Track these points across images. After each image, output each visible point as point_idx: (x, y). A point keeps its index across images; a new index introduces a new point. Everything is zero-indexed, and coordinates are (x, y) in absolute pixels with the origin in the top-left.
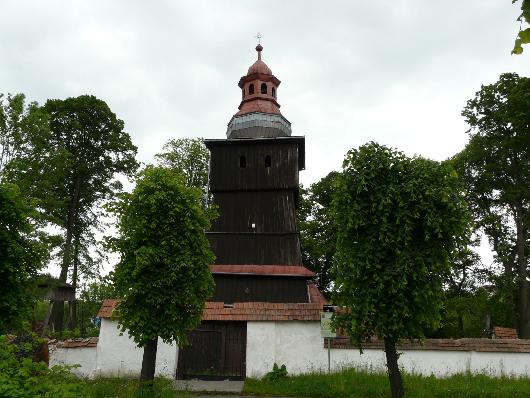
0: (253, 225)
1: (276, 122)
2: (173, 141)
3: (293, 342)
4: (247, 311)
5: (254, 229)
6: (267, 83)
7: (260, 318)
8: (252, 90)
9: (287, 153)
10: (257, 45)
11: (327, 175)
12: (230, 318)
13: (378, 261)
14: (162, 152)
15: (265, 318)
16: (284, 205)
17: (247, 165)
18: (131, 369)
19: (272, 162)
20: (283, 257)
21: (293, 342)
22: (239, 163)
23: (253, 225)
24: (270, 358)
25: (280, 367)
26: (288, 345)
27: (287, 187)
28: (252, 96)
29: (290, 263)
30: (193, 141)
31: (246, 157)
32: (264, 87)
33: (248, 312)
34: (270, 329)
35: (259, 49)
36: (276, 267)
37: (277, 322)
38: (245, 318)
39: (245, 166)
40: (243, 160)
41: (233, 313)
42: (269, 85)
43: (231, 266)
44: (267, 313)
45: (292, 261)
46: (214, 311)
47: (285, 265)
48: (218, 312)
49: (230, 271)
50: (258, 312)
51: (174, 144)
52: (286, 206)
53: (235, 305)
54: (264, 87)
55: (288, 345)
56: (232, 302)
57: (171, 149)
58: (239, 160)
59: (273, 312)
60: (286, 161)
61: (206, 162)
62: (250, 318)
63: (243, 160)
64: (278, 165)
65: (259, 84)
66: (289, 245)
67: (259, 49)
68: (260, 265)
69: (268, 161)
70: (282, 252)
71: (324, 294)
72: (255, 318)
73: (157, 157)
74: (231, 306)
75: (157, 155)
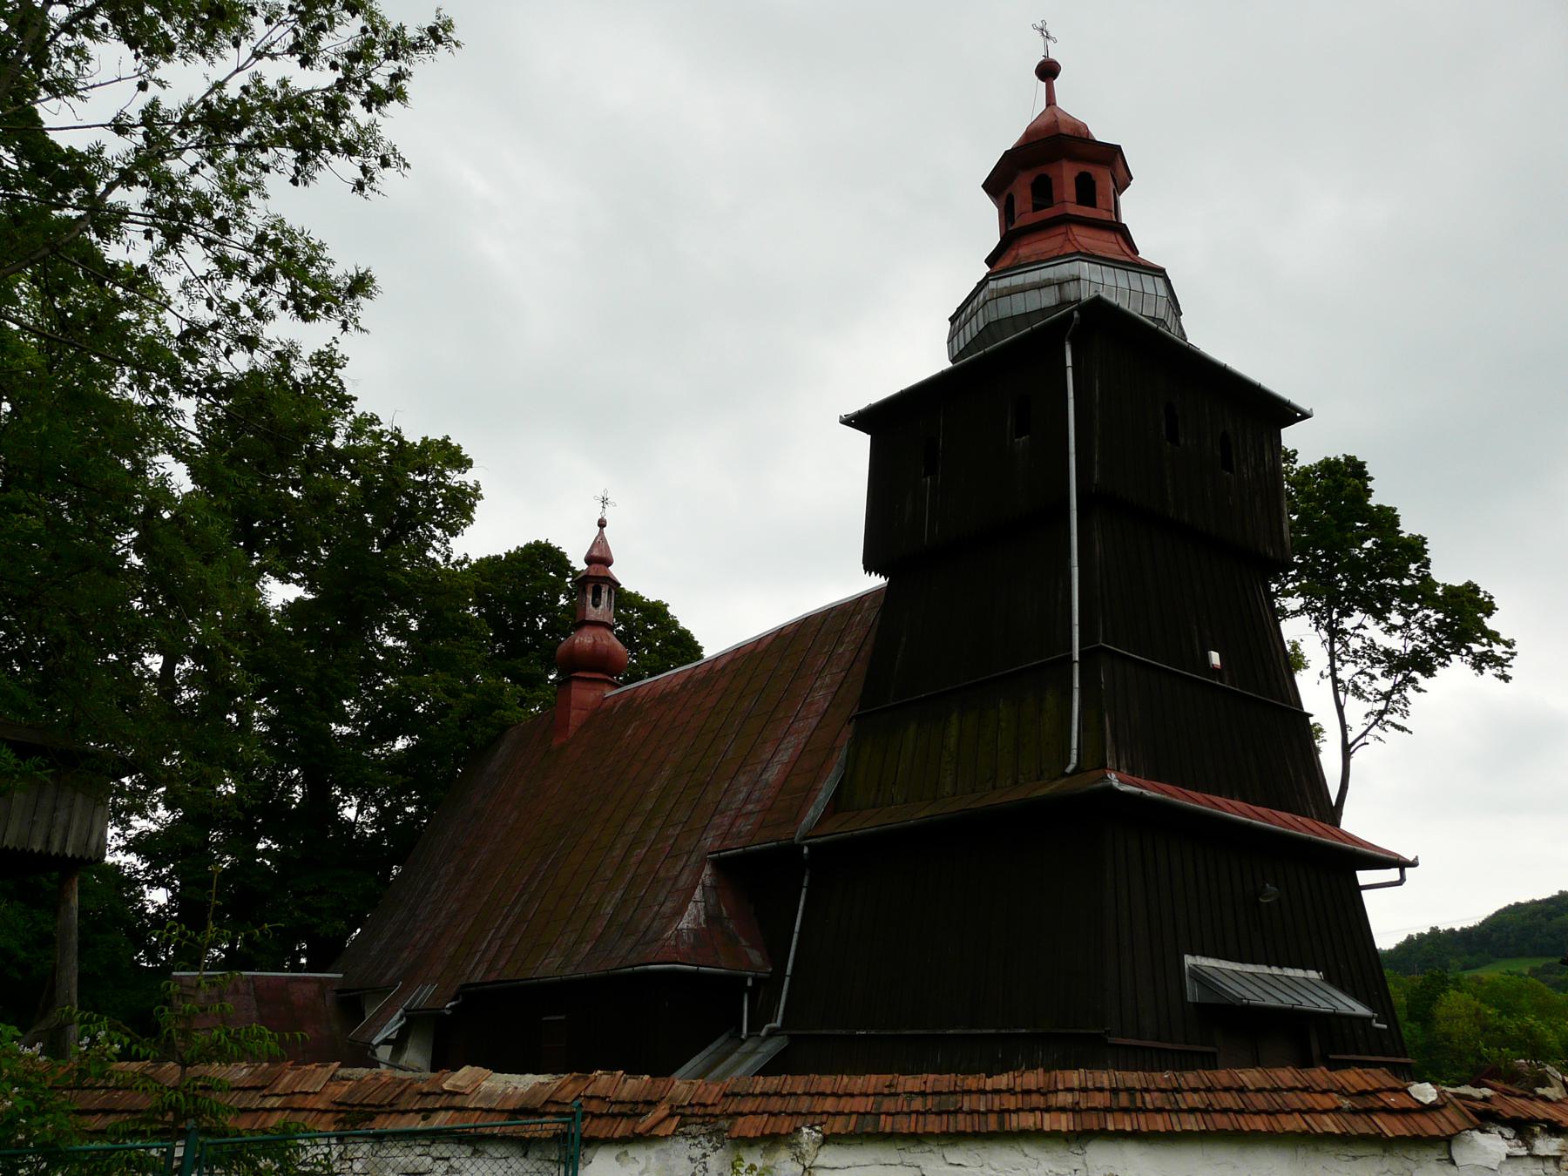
8: (1043, 192)
35: (1047, 71)
42: (1103, 178)
65: (1066, 175)
67: (1047, 71)
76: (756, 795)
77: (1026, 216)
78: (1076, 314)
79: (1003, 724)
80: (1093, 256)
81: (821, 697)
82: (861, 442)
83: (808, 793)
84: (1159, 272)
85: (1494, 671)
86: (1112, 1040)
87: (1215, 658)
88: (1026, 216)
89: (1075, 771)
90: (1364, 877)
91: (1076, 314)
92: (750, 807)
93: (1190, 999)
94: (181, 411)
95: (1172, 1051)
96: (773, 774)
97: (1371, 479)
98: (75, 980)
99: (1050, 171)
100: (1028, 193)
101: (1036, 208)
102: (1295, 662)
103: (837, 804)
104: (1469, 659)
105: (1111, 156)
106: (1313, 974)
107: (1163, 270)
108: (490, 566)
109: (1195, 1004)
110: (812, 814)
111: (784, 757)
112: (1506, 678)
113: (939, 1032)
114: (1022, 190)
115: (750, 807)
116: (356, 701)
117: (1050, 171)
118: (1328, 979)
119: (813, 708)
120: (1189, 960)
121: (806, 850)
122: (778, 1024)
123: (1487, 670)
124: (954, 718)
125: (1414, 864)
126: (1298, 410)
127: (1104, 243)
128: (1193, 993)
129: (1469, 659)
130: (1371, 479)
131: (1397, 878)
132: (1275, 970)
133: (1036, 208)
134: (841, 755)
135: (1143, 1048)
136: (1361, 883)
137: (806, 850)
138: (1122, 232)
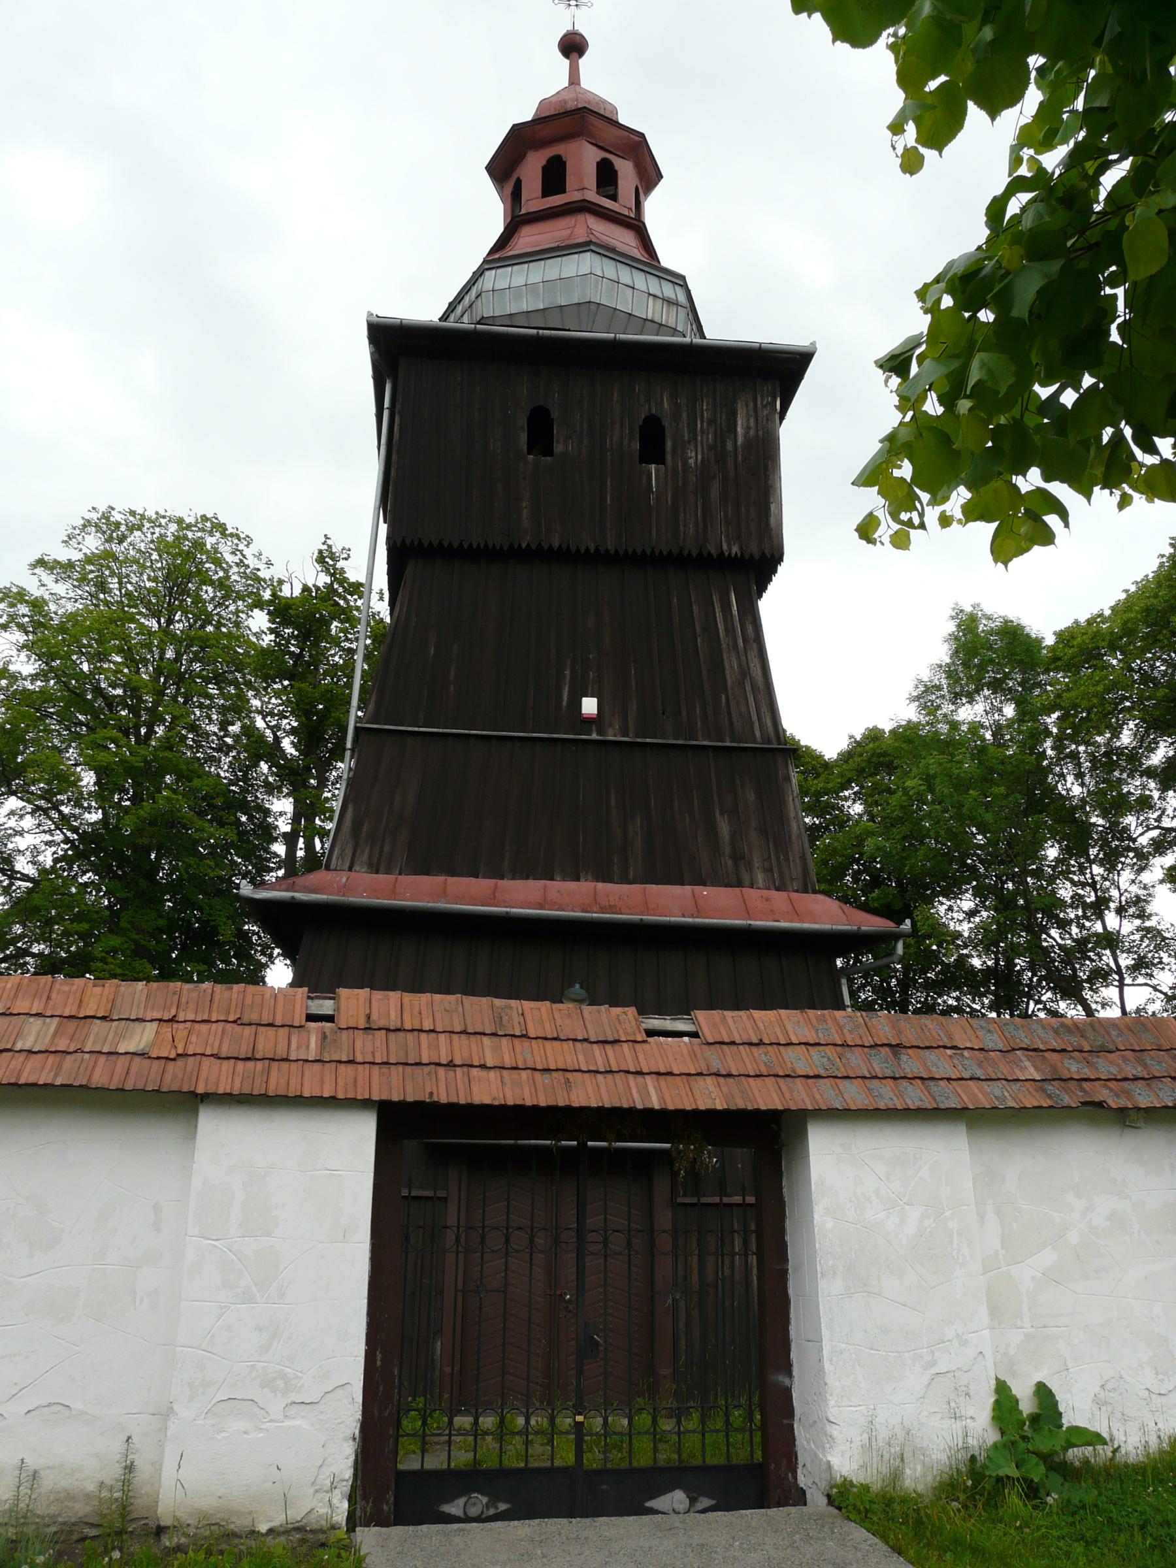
0: (589, 706)
1: (669, 302)
2: (106, 517)
3: (1073, 1237)
4: (790, 1054)
5: (589, 721)
6: (618, 163)
7: (886, 1096)
8: (555, 177)
9: (733, 414)
10: (532, 84)
11: (769, 587)
12: (710, 1096)
13: (961, 916)
14: (64, 554)
15: (914, 1096)
16: (721, 626)
17: (558, 448)
18: (32, 1462)
19: (669, 444)
20: (727, 851)
21: (1073, 1237)
22: (524, 437)
23: (589, 706)
24: (964, 1343)
25: (1027, 1406)
26: (1048, 1257)
27: (735, 549)
28: (556, 200)
29: (760, 877)
30: (180, 521)
31: (555, 414)
32: (607, 177)
33: (796, 1059)
34: (941, 1162)
35: (573, 46)
36: (705, 892)
37: (977, 1118)
38: (799, 1097)
39: (549, 452)
40: (541, 432)
41: (716, 1065)
42: (625, 169)
43: (491, 883)
44: (910, 1064)
45: (769, 871)
46: (599, 1057)
47: (739, 884)
48: (625, 1056)
49: (492, 900)
50: (856, 1061)
51: (107, 526)
52: (730, 630)
53: (706, 1020)
54: (607, 177)
55: (1048, 1257)
56: (683, 1009)
57: (93, 543)
58: (522, 421)
59: (939, 1064)
60: (729, 446)
61: (220, 605)
62: (827, 1095)
63: (541, 432)
64: (694, 457)
65: (583, 159)
66: (751, 797)
67: (573, 46)
68: (625, 880)
69: (652, 440)
70: (724, 828)
71: (916, 1012)
72: (854, 1095)
73: (38, 571)
74: (681, 1026)
75: (41, 563)
77: (533, 201)
80: (613, 250)
84: (679, 280)
88: (533, 201)
94: (321, 559)
97: (809, 16)
101: (546, 193)
102: (1086, 1462)
105: (636, 147)
107: (683, 278)
108: (402, 557)
114: (532, 170)
116: (1141, 776)
127: (624, 240)
130: (809, 16)
133: (546, 193)
138: (638, 228)
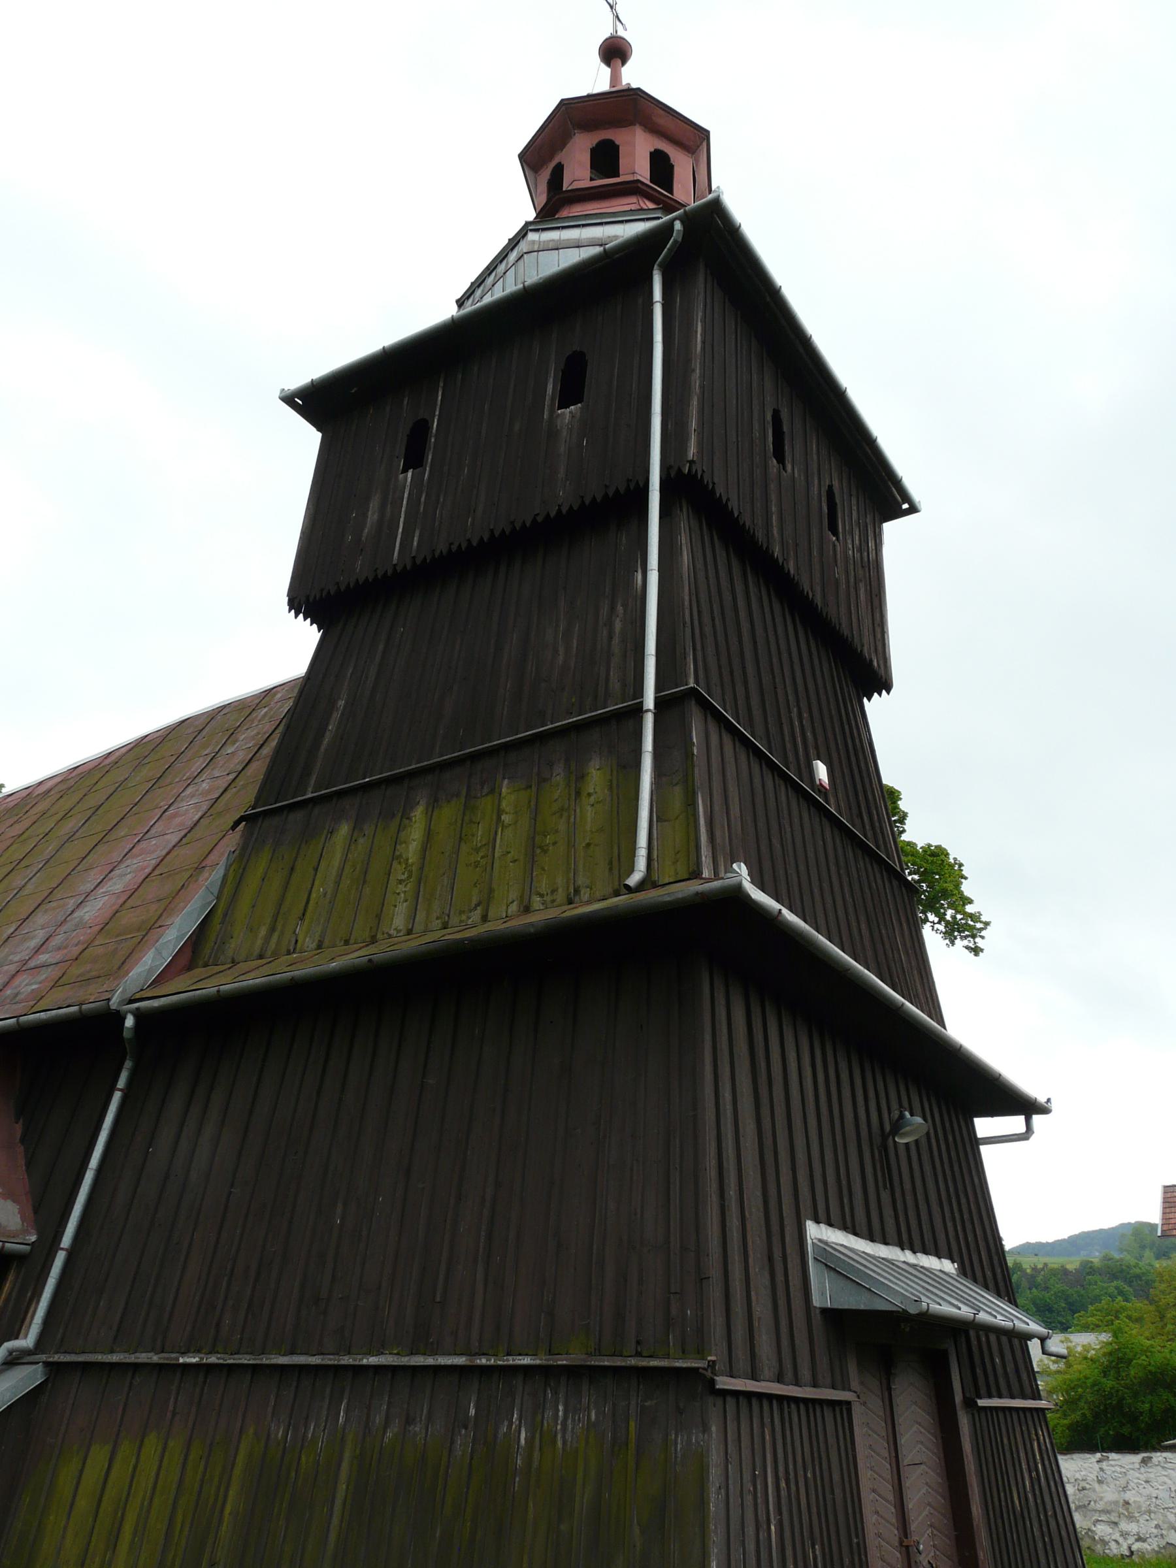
76: (56, 941)
78: (678, 226)
79: (506, 818)
81: (190, 808)
82: (307, 440)
83: (149, 930)
85: (965, 943)
86: (724, 1382)
87: (822, 771)
89: (642, 886)
90: (984, 1126)
91: (678, 226)
92: (43, 958)
93: (817, 1301)
95: (796, 1400)
96: (92, 912)
98: (694, 1365)
99: (619, 136)
100: (586, 158)
103: (194, 951)
104: (941, 927)
106: (949, 1266)
109: (825, 1311)
110: (151, 961)
111: (118, 885)
112: (976, 951)
113: (346, 1360)
115: (43, 958)
117: (619, 136)
118: (965, 1271)
119: (178, 820)
120: (815, 1231)
121: (129, 1022)
122: (28, 1341)
123: (958, 941)
124: (418, 813)
125: (1044, 1110)
126: (906, 497)
128: (824, 1292)
129: (941, 927)
131: (1022, 1129)
132: (909, 1257)
133: (592, 179)
134: (214, 876)
135: (760, 1396)
136: (980, 1135)
137: (129, 1022)
